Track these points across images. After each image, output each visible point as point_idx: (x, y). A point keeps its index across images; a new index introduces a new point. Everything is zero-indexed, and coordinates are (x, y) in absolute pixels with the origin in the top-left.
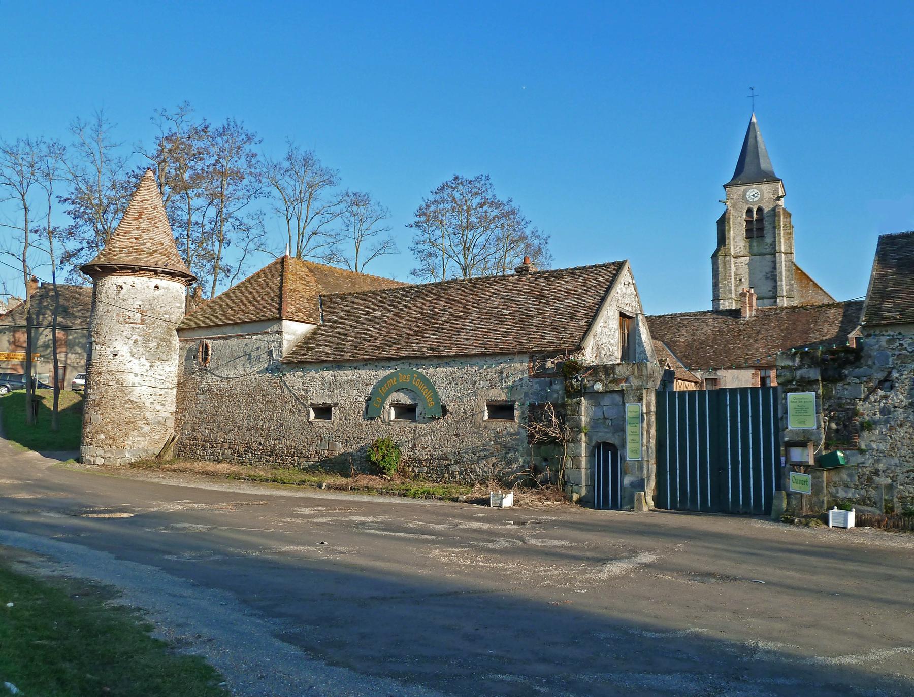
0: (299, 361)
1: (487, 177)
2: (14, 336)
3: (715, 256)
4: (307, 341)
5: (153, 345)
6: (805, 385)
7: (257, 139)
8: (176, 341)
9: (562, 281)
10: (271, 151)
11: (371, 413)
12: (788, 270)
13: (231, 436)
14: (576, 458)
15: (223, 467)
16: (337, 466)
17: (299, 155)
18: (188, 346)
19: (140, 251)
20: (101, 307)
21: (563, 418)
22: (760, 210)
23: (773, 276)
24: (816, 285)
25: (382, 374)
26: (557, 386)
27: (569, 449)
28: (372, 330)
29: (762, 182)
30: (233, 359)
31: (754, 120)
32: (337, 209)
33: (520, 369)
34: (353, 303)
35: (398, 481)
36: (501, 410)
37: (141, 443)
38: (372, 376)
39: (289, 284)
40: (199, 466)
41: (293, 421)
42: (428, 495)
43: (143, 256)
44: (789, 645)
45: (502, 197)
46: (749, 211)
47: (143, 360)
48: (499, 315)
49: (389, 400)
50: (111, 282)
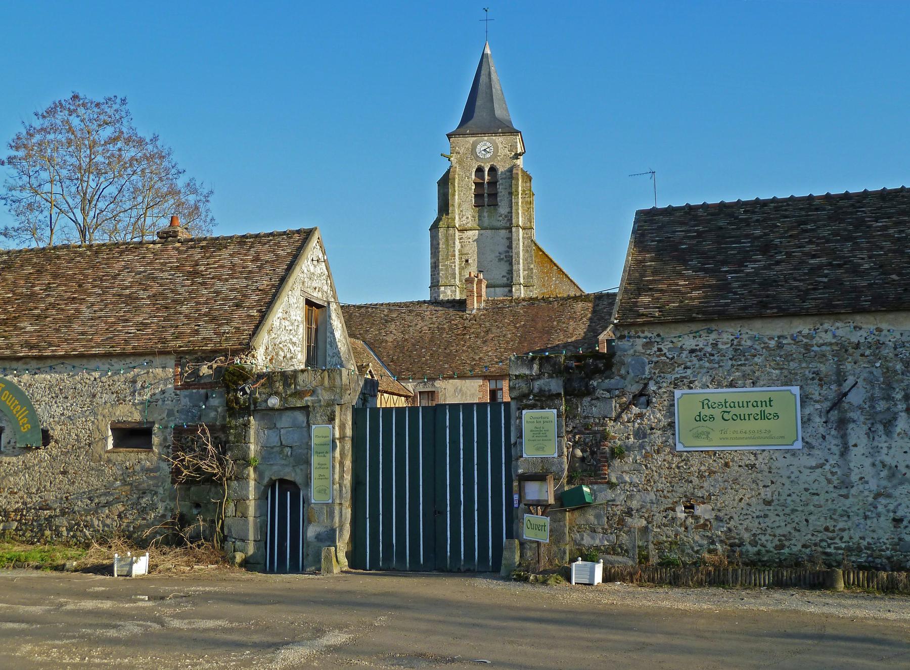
1: (124, 101)
3: (435, 227)
9: (225, 253)
12: (526, 251)
14: (240, 501)
22: (493, 169)
23: (508, 259)
26: (215, 401)
27: (231, 489)
29: (496, 133)
31: (488, 51)
33: (162, 376)
46: (480, 170)
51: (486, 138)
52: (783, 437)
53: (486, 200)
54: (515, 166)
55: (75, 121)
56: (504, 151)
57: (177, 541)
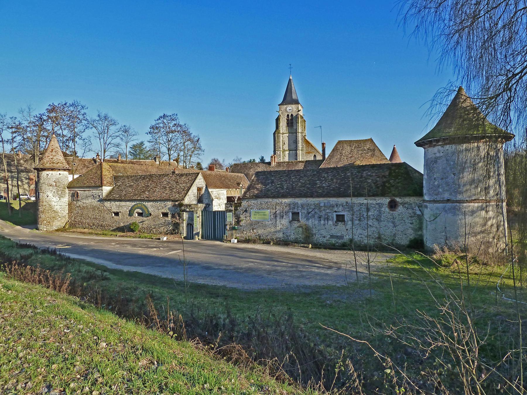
0: (109, 198)
1: (177, 115)
3: (274, 134)
4: (110, 192)
5: (60, 193)
6: (231, 211)
7: (86, 108)
8: (67, 190)
9: (183, 177)
10: (92, 115)
11: (131, 214)
13: (87, 221)
14: (183, 227)
15: (86, 230)
16: (121, 229)
17: (103, 115)
18: (71, 192)
19: (53, 163)
21: (179, 216)
22: (292, 115)
23: (296, 142)
24: (312, 145)
25: (133, 204)
26: (178, 209)
27: (181, 225)
28: (130, 190)
29: (292, 104)
30: (87, 197)
31: (291, 78)
32: (117, 134)
33: (170, 204)
34: (124, 180)
35: (138, 233)
36: (165, 215)
37: (58, 224)
38: (131, 204)
39: (104, 173)
40: (79, 230)
41: (107, 217)
42: (146, 238)
43: (55, 165)
45: (182, 123)
46: (288, 115)
47: (57, 198)
48: (165, 188)
49: (135, 211)
50: (44, 173)
54: (298, 114)
55: (165, 121)
56: (295, 110)
57: (172, 234)
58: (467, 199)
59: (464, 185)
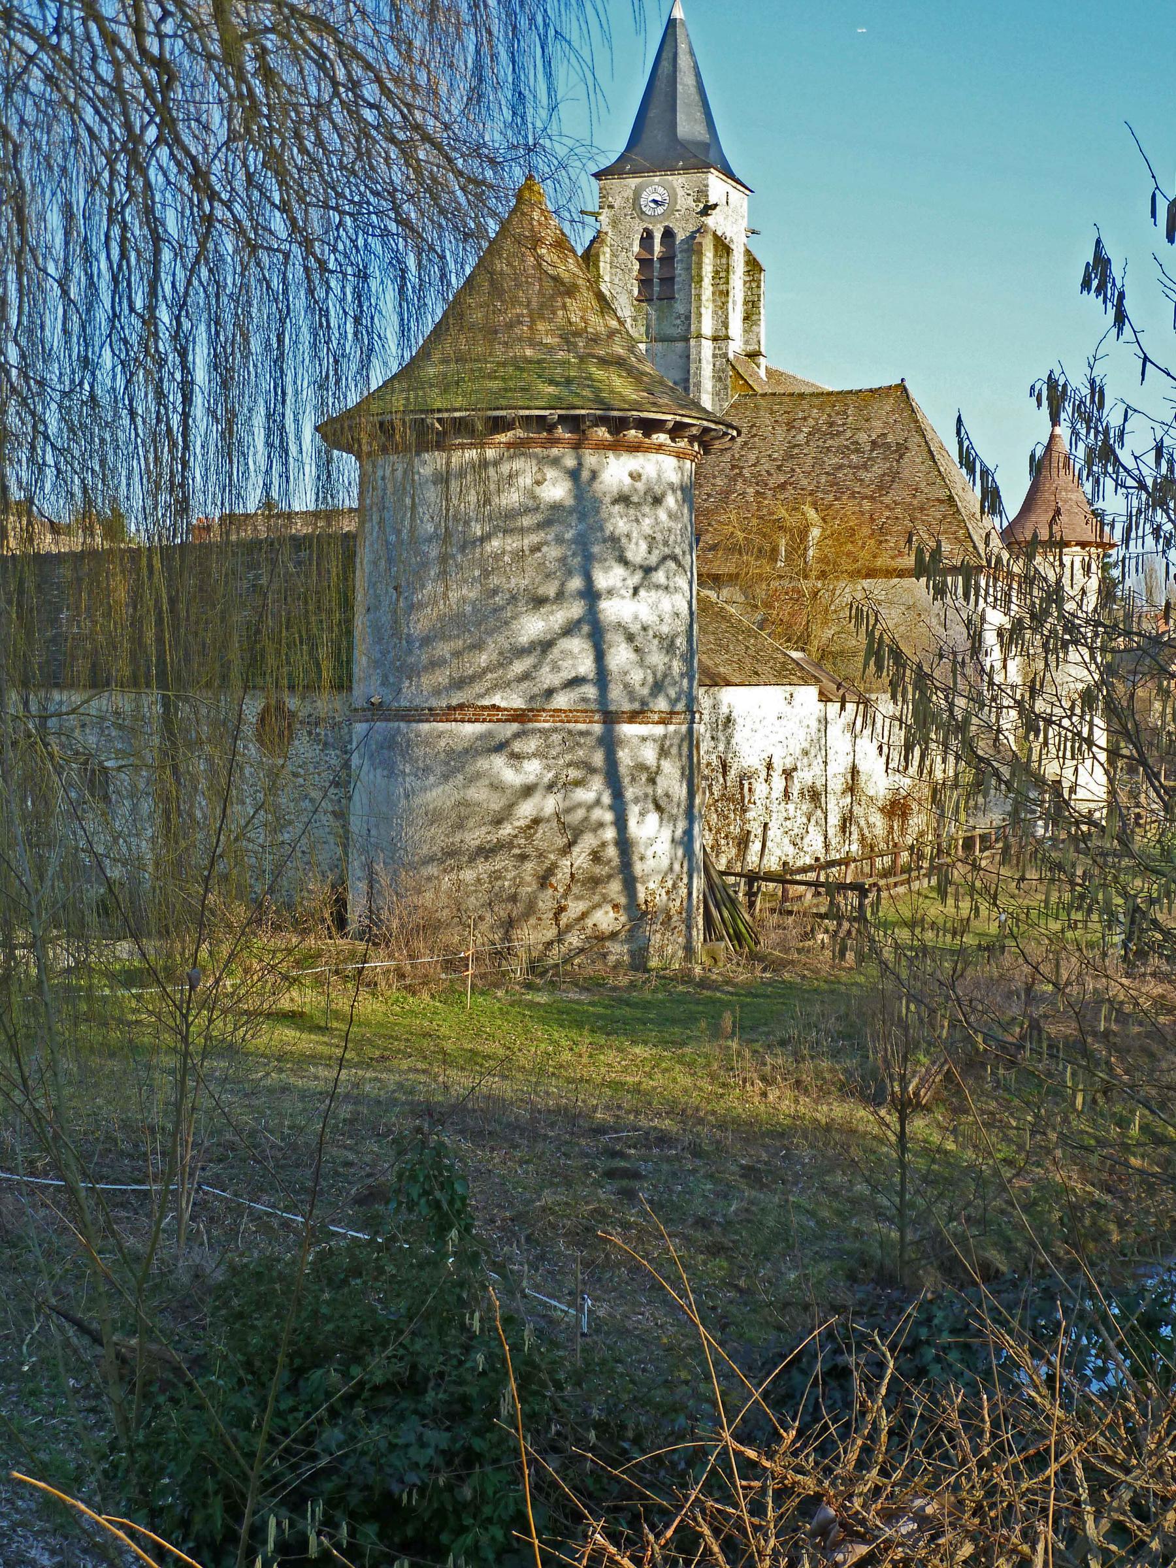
2: (330, 1001)
12: (718, 378)
20: (863, 778)
22: (668, 234)
29: (672, 170)
31: (678, 13)
44: (71, 1333)
51: (657, 179)
52: (1098, 276)
53: (656, 289)
54: (701, 230)
56: (685, 202)
58: (434, 702)
59: (426, 641)
